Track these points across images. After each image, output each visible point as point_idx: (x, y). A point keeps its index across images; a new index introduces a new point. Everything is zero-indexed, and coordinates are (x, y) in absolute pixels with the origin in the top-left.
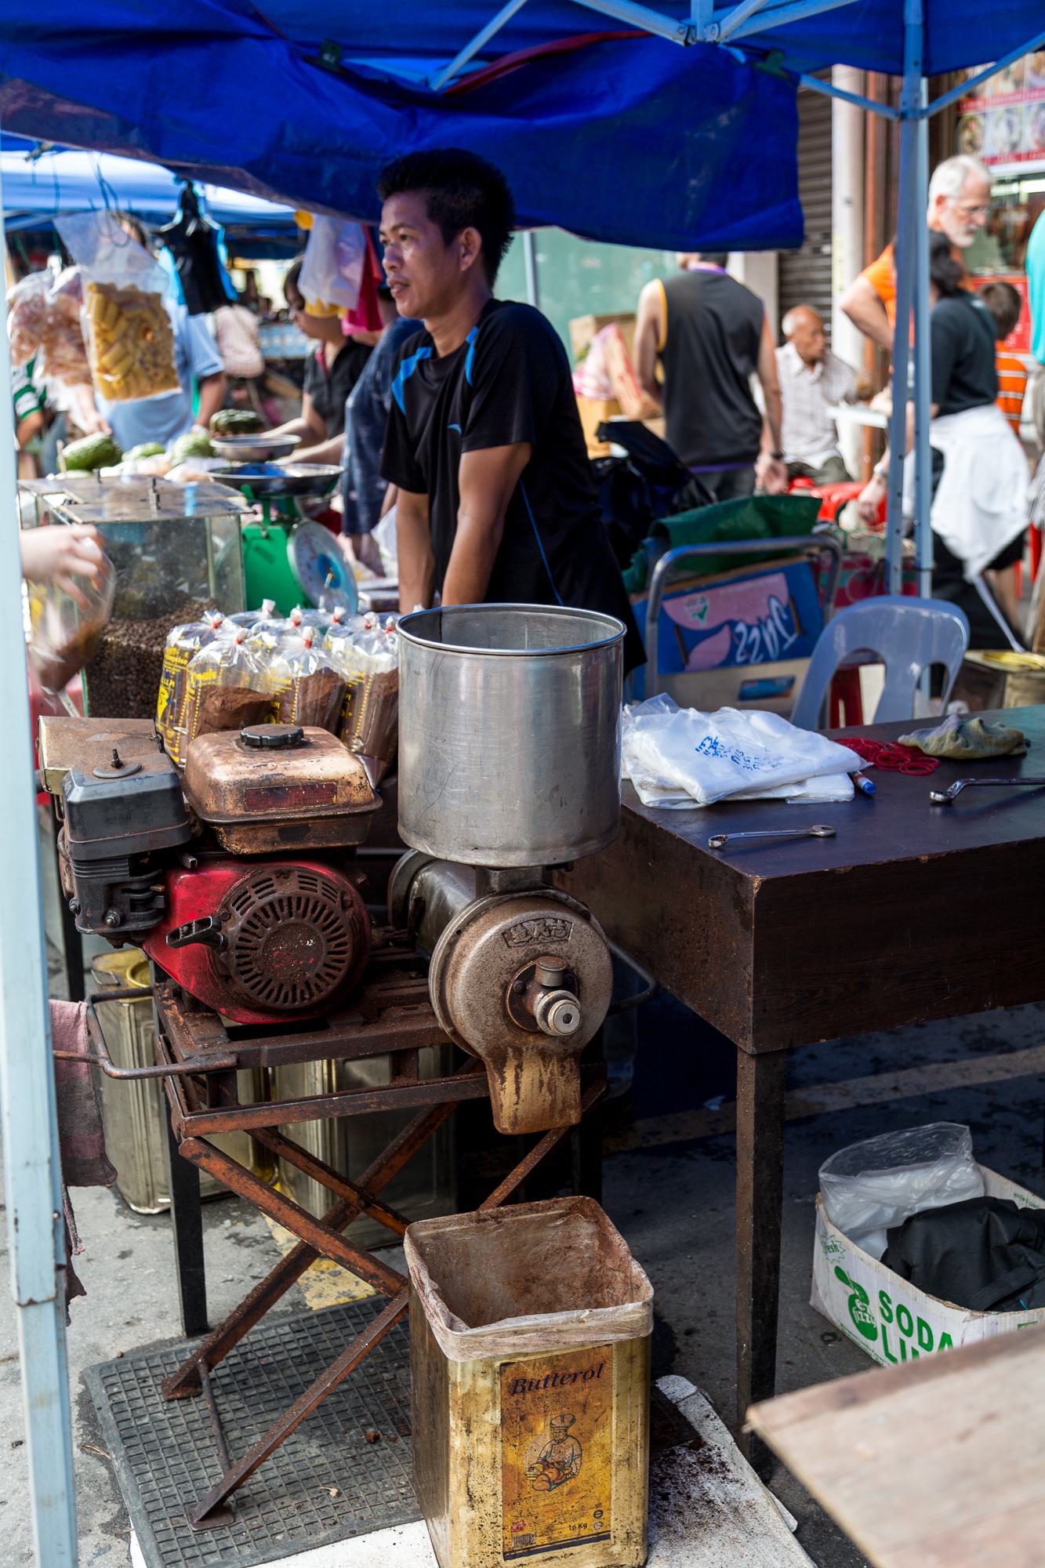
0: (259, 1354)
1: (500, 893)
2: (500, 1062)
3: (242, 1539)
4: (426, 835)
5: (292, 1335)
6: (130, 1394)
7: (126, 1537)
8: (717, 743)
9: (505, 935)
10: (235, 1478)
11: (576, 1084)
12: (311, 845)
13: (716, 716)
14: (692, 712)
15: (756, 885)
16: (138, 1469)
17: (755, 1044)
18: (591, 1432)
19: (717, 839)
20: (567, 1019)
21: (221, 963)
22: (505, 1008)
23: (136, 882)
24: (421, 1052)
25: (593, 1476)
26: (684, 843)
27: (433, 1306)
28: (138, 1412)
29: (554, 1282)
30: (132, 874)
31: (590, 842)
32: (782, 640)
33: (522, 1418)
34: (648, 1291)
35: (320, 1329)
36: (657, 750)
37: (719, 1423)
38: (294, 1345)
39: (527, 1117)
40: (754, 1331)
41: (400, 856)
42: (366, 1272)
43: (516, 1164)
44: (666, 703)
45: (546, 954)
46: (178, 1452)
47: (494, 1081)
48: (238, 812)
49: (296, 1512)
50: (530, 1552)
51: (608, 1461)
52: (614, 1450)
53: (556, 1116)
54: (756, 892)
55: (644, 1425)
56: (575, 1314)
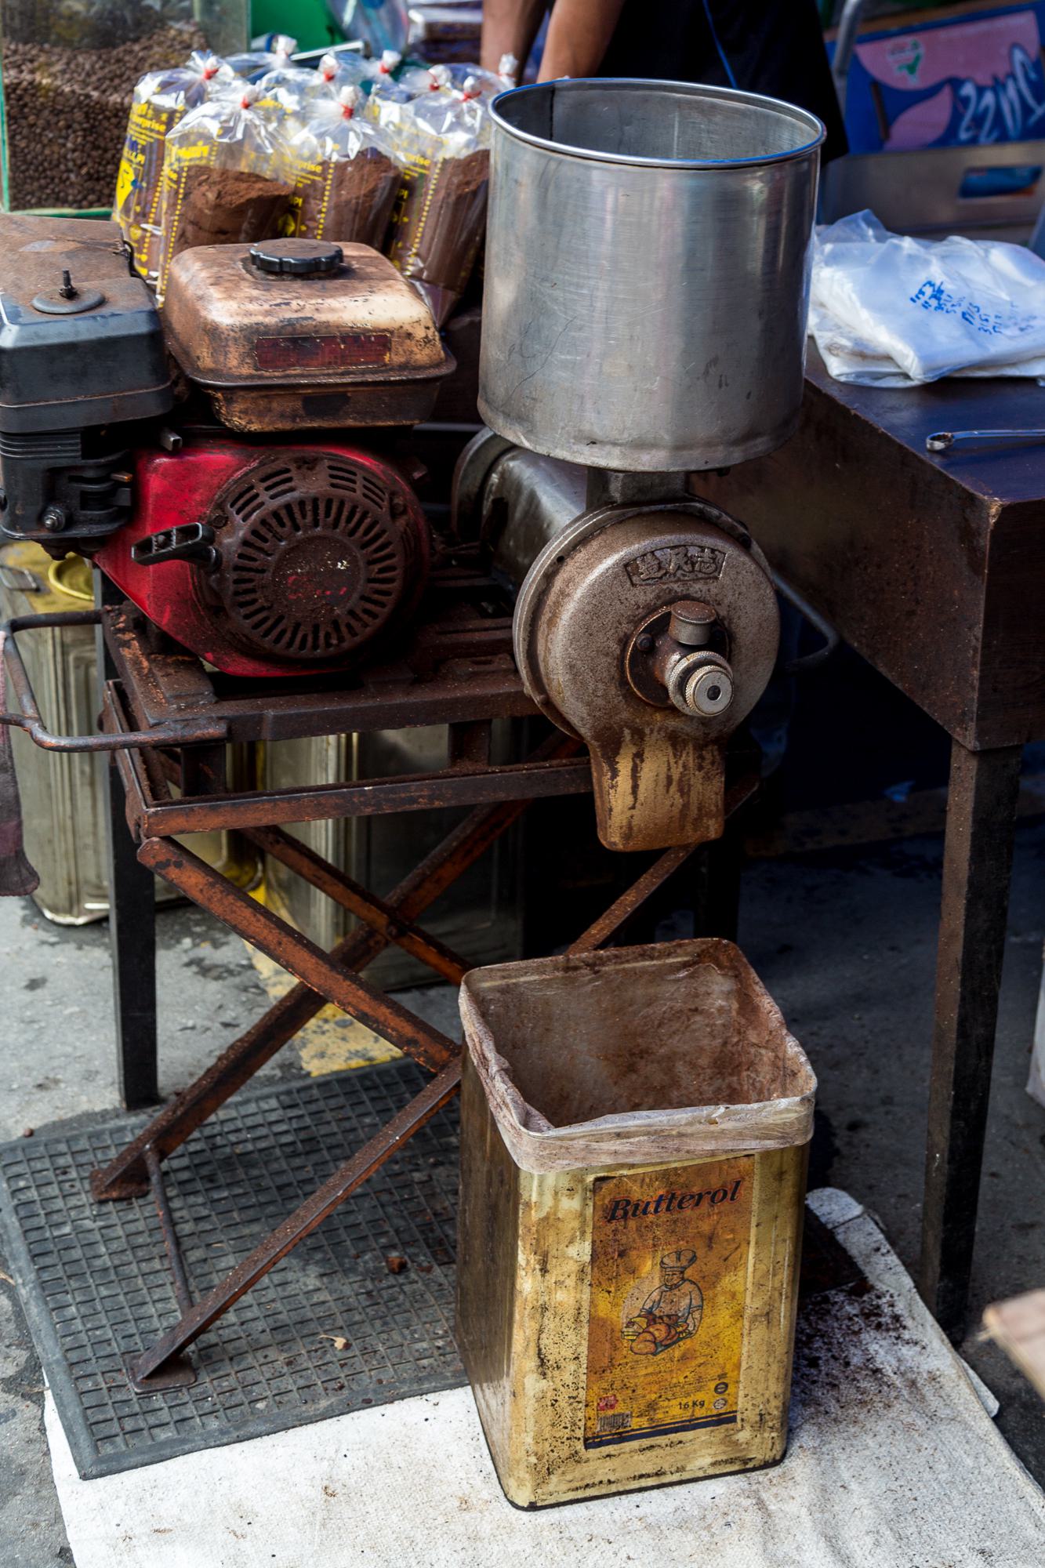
0: (233, 1138)
1: (624, 505)
2: (612, 747)
3: (207, 1406)
4: (521, 418)
5: (281, 1112)
6: (43, 1190)
7: (39, 1400)
8: (940, 291)
9: (628, 568)
10: (199, 1321)
11: (718, 783)
12: (350, 422)
13: (940, 248)
14: (908, 244)
15: (993, 511)
16: (57, 1301)
17: (980, 734)
18: (718, 1276)
19: (938, 438)
20: (714, 693)
21: (210, 588)
22: (622, 672)
23: (90, 467)
24: (494, 721)
25: (717, 1336)
26: (889, 441)
27: (500, 1092)
28: (56, 1218)
29: (671, 1058)
30: (84, 457)
31: (759, 440)
32: (1027, 110)
33: (622, 1254)
34: (808, 1080)
35: (321, 1105)
36: (854, 297)
37: (893, 1259)
38: (283, 1127)
39: (647, 828)
40: (953, 1137)
41: (473, 434)
42: (400, 1036)
43: (622, 891)
44: (869, 224)
45: (686, 597)
46: (113, 1277)
47: (601, 774)
48: (246, 370)
49: (285, 1370)
50: (621, 1438)
51: (739, 1315)
52: (748, 1301)
53: (689, 828)
54: (993, 521)
55: (793, 1266)
56: (705, 1111)
